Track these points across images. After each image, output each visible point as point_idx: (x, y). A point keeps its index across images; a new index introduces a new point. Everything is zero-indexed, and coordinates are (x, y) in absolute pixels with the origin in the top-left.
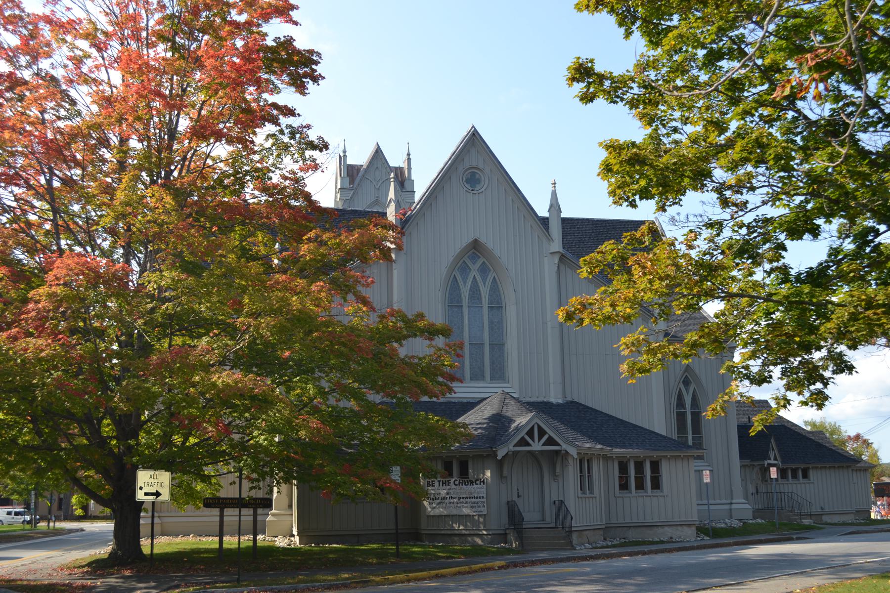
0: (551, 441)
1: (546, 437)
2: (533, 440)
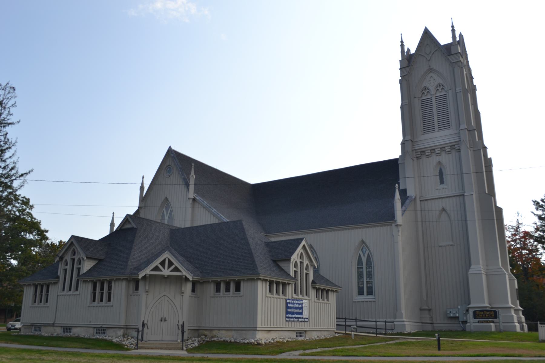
0: (176, 269)
1: (173, 267)
2: (164, 268)
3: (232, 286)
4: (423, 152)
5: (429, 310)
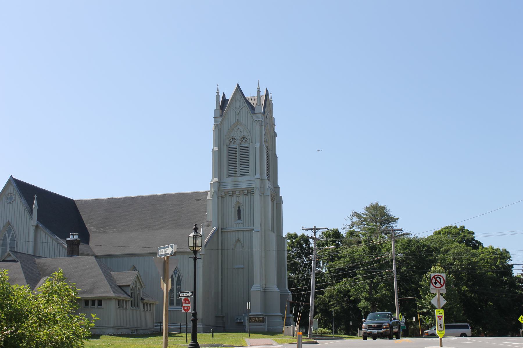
3: (96, 303)
4: (226, 193)
5: (223, 317)
